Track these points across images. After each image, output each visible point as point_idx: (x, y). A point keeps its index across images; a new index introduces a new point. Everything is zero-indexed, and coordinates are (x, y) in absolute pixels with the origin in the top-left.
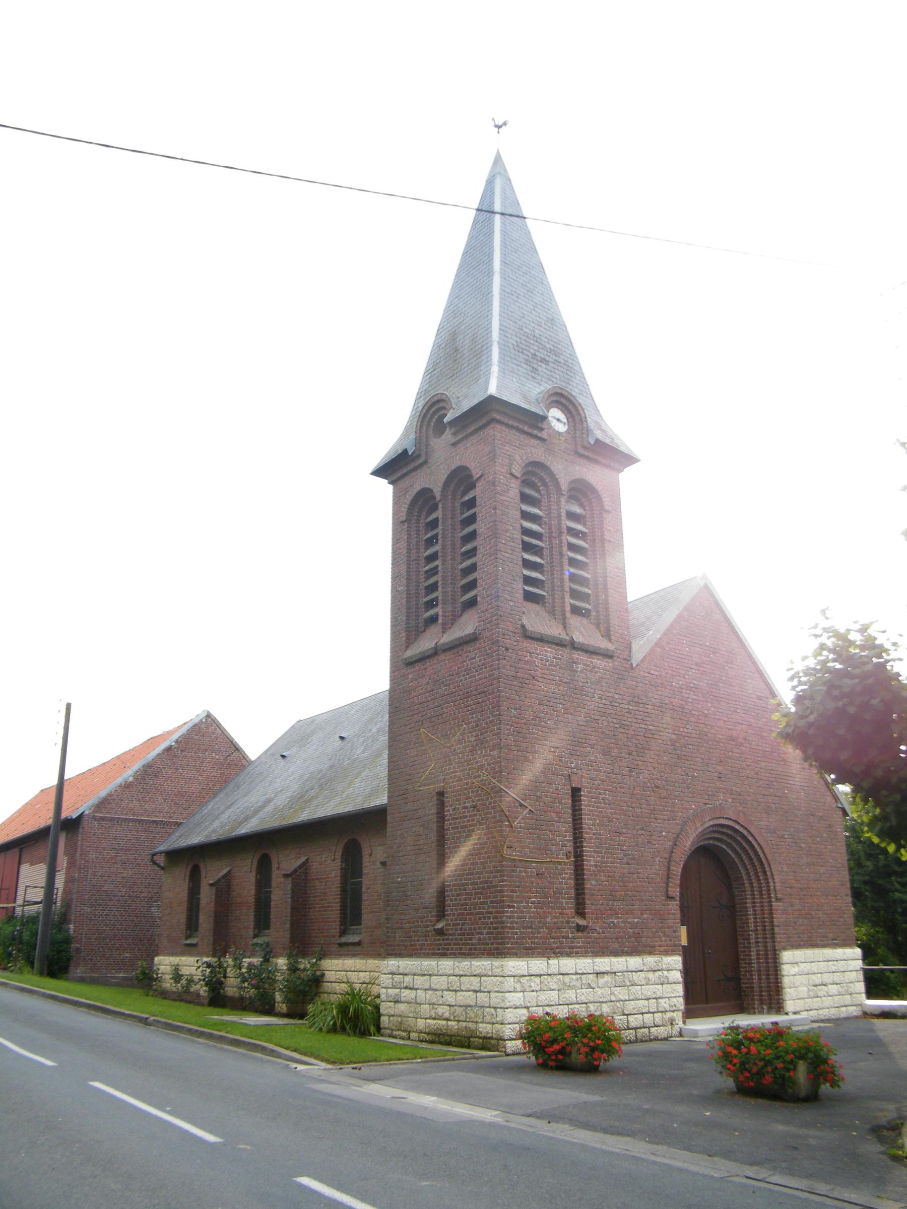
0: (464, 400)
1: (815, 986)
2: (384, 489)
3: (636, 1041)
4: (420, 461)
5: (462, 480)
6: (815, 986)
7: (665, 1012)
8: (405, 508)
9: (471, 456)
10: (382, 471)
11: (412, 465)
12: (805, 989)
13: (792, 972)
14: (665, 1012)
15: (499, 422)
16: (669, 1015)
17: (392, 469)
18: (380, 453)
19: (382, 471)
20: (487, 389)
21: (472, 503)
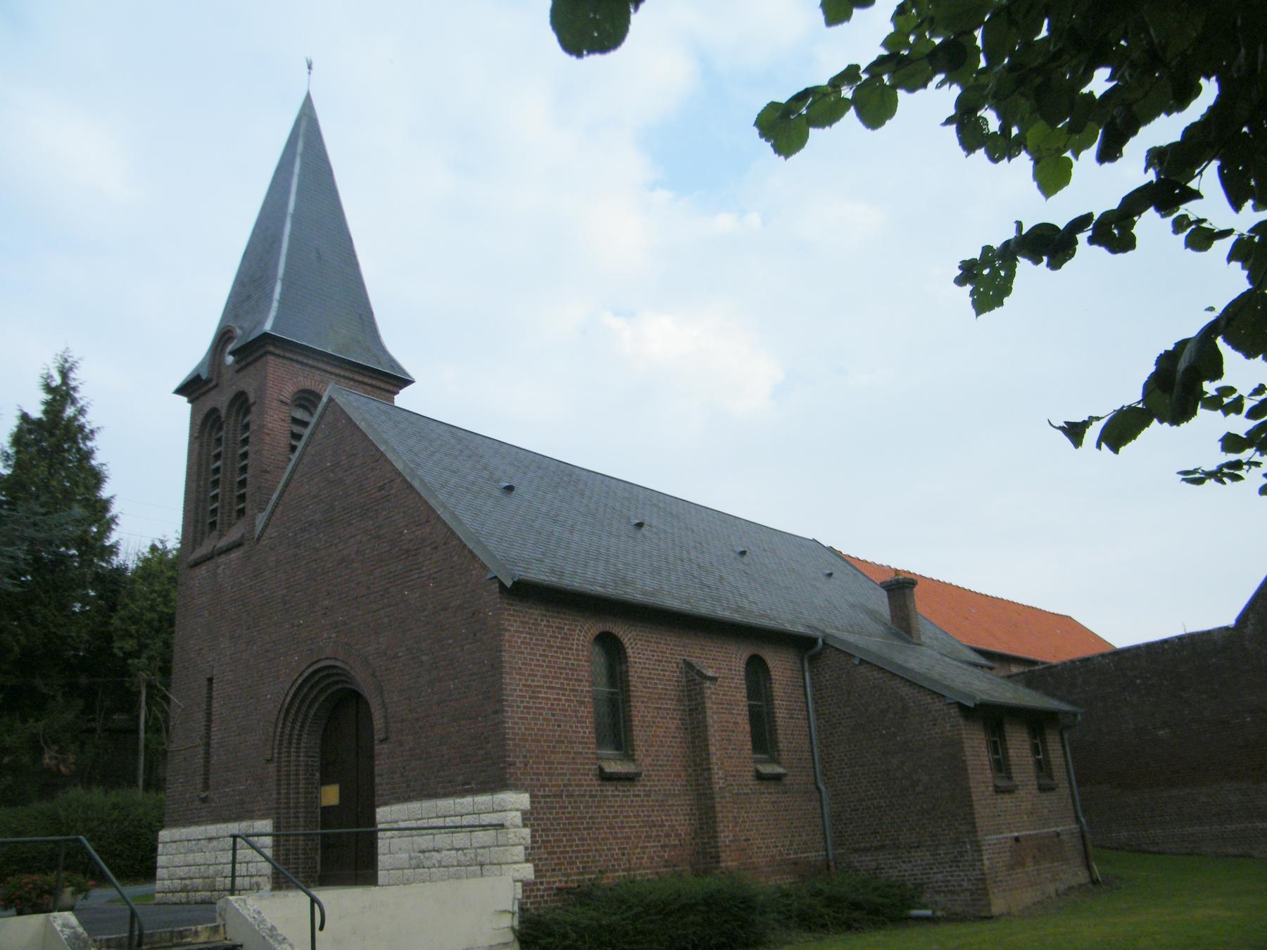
0: (242, 336)
1: (423, 852)
2: (183, 407)
3: (188, 903)
4: (211, 385)
5: (241, 402)
6: (423, 852)
7: (252, 876)
8: (199, 422)
9: (247, 383)
10: (181, 391)
11: (206, 388)
12: (405, 856)
13: (514, 813)
14: (252, 876)
15: (273, 354)
16: (254, 880)
17: (191, 388)
18: (182, 374)
19: (181, 391)
20: (262, 323)
21: (246, 427)
